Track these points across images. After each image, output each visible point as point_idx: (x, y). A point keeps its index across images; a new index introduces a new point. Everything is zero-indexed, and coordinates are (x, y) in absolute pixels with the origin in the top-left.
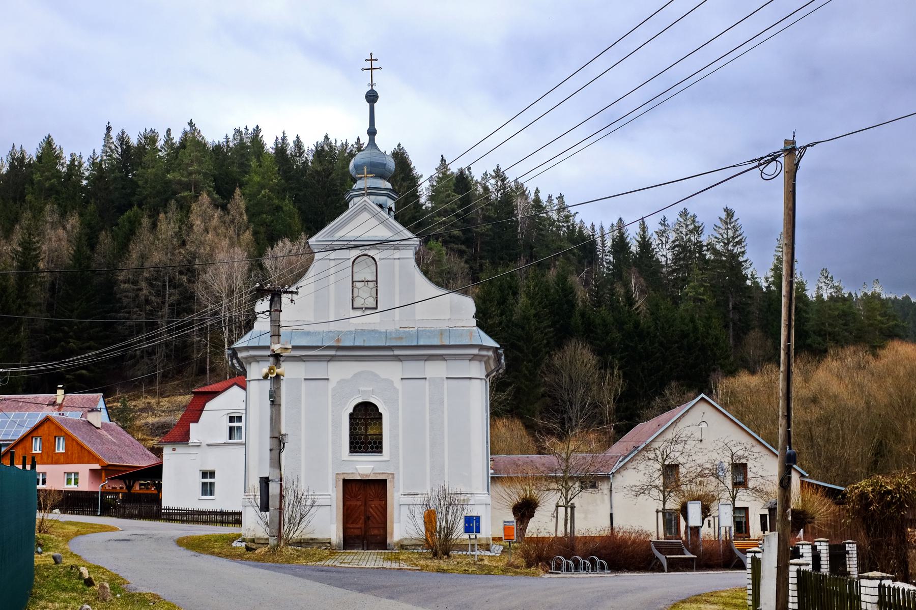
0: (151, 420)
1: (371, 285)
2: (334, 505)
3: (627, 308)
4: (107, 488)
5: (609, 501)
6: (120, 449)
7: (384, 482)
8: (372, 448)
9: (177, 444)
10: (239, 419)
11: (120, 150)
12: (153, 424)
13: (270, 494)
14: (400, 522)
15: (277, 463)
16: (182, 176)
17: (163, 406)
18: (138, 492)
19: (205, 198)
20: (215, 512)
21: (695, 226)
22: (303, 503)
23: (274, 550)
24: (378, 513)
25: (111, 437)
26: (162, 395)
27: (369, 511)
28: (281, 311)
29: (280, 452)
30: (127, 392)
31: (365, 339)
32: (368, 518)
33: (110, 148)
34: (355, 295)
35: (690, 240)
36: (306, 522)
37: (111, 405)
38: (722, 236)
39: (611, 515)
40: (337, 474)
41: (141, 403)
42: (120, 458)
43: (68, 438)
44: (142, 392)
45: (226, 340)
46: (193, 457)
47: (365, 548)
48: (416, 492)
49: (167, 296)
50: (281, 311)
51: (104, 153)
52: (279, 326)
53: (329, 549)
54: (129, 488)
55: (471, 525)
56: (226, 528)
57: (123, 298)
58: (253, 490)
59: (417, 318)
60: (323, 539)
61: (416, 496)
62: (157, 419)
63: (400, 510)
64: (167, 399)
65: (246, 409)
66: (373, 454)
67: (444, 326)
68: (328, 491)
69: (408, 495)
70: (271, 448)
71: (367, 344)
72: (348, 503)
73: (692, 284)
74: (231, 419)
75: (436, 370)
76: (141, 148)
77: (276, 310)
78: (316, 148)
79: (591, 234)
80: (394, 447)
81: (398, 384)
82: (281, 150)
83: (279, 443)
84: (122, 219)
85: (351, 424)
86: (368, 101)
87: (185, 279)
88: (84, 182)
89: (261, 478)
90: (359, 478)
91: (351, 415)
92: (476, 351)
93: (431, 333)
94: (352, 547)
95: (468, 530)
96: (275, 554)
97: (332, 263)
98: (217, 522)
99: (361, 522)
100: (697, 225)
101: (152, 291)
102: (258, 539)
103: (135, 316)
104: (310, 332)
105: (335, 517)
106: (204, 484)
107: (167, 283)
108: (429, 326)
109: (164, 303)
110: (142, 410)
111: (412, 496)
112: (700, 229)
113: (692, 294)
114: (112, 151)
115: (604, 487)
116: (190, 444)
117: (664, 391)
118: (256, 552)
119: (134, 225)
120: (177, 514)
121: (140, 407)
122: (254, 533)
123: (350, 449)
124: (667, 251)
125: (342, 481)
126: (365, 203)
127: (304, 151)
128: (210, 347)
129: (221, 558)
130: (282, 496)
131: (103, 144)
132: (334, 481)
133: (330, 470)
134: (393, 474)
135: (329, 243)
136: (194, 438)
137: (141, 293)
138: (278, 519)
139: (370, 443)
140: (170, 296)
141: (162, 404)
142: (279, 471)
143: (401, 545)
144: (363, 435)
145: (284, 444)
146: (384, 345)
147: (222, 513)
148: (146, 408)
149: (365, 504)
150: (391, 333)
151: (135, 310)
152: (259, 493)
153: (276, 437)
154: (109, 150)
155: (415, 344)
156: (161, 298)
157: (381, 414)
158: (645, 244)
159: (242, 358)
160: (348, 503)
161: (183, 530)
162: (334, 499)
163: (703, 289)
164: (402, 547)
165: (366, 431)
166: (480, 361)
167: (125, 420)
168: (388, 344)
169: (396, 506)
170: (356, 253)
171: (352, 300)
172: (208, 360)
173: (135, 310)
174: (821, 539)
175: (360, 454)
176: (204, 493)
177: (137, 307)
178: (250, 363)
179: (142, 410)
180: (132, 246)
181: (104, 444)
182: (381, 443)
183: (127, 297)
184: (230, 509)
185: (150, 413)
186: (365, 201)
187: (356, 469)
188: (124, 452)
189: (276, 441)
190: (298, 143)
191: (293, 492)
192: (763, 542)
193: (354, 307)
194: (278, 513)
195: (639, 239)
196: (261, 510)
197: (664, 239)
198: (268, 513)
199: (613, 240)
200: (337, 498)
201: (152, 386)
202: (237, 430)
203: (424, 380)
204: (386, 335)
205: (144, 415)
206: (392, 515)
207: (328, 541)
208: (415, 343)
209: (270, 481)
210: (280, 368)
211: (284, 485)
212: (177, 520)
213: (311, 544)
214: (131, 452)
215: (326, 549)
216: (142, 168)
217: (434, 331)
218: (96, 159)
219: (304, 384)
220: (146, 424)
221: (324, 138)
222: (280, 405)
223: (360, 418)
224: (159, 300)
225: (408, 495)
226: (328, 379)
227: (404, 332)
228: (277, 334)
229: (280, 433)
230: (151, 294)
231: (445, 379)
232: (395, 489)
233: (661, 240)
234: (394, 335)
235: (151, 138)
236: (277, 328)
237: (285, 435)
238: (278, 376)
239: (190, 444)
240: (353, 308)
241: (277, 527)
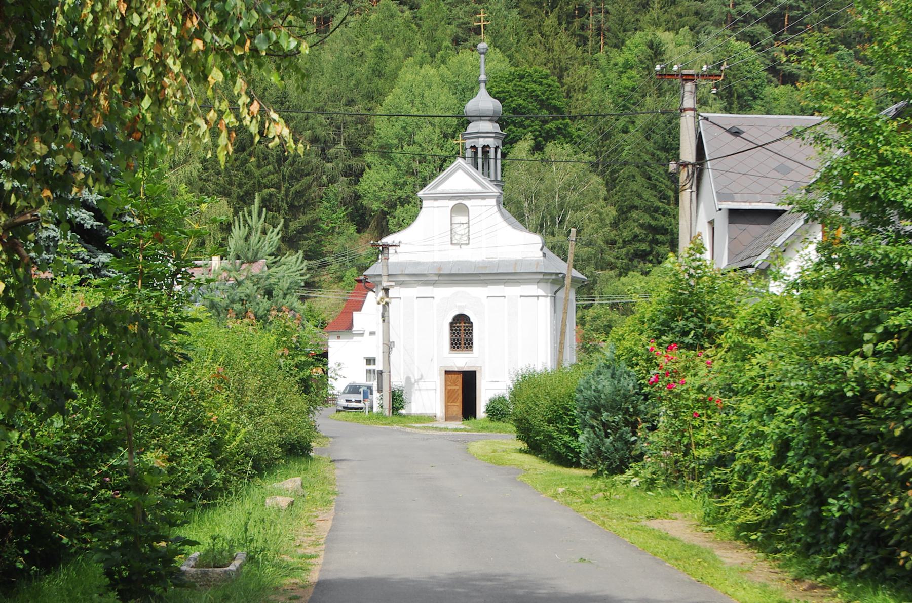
1: (466, 226)
71: (460, 272)
75: (513, 291)
92: (541, 277)
97: (484, 209)
136: (356, 327)
157: (472, 323)
170: (453, 203)
204: (475, 264)
226: (433, 298)
227: (489, 261)
234: (481, 265)
238: (387, 303)
240: (452, 244)
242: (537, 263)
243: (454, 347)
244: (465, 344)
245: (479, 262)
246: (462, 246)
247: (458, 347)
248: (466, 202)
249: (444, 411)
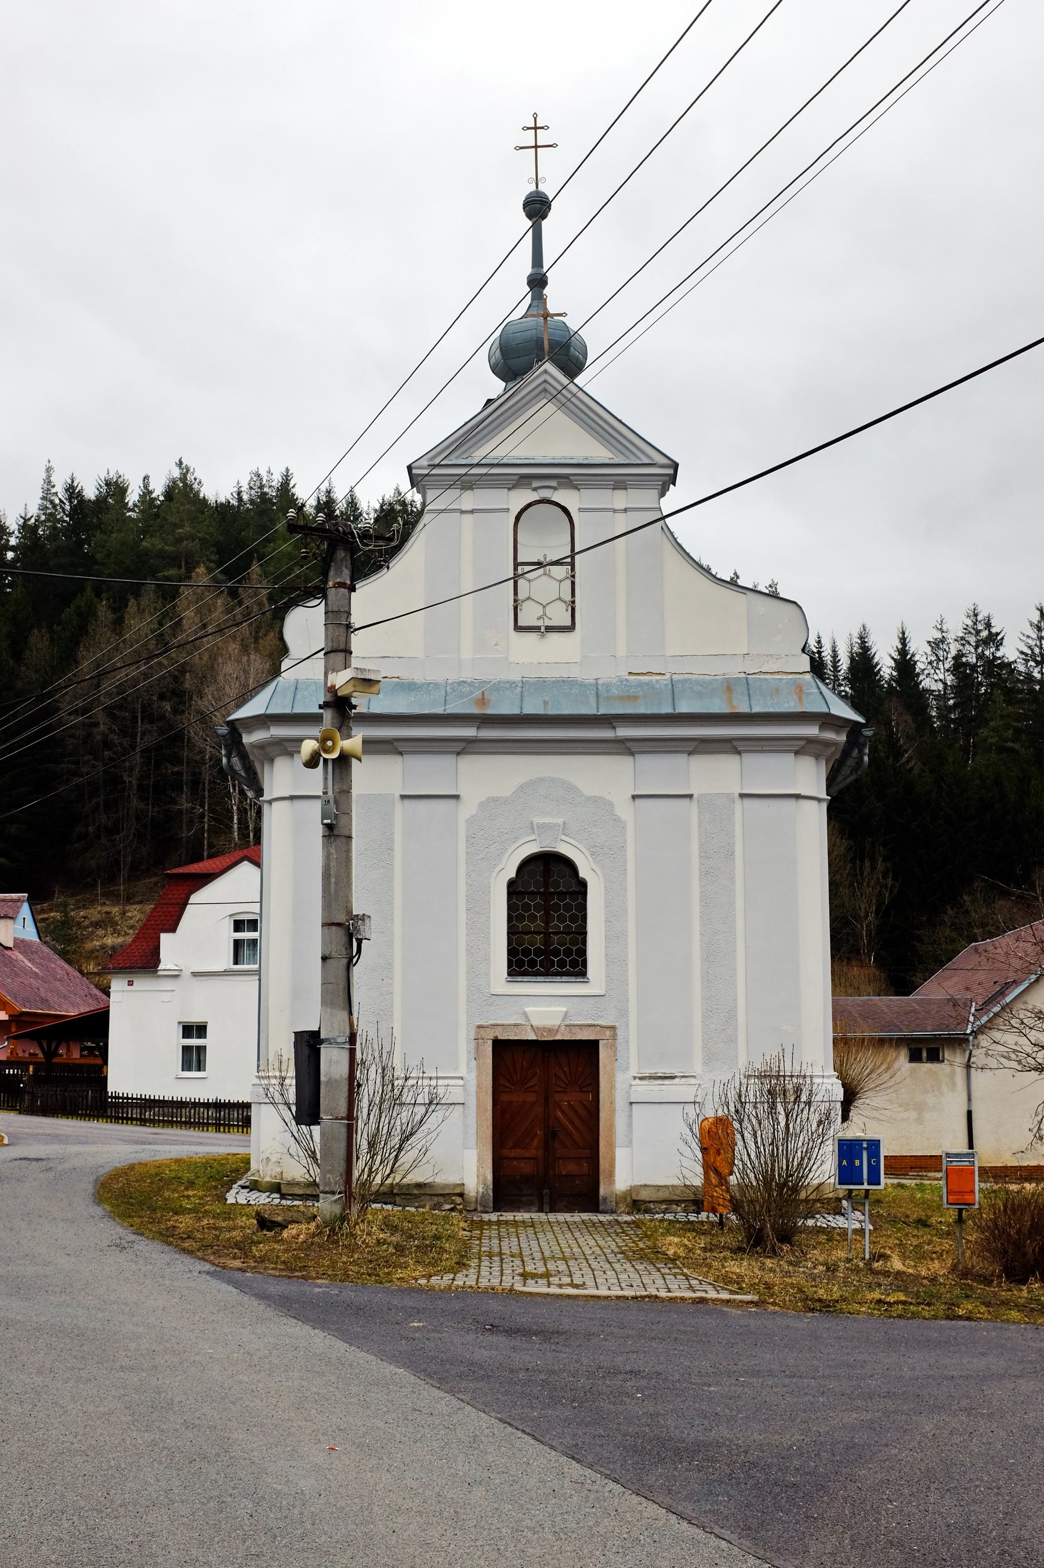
0: (109, 941)
2: (472, 1102)
3: (891, 760)
4: (21, 1054)
5: (965, 1089)
6: (46, 985)
7: (591, 1048)
8: (562, 964)
9: (135, 973)
10: (253, 925)
11: (68, 507)
12: (113, 948)
13: (323, 1078)
14: (630, 1144)
15: (342, 999)
16: (166, 543)
17: (131, 918)
18: (77, 1062)
19: (202, 575)
20: (204, 1103)
21: (990, 633)
22: (407, 1098)
23: (332, 1230)
24: (577, 1122)
25: (30, 965)
26: (129, 899)
27: (557, 1118)
29: (349, 964)
30: (73, 895)
31: (547, 699)
32: (551, 1135)
33: (52, 502)
34: (521, 597)
35: (984, 654)
36: (415, 1151)
37: (46, 916)
38: (1032, 650)
39: (969, 1114)
40: (479, 1027)
41: (94, 913)
42: (44, 1001)
44: (97, 895)
45: (235, 808)
46: (166, 996)
47: (546, 1207)
48: (668, 1071)
49: (139, 734)
51: (42, 510)
52: (348, 626)
53: (461, 1212)
54: (50, 1054)
55: (857, 1163)
56: (226, 1136)
57: (67, 738)
58: (277, 1066)
59: (670, 652)
60: (447, 1186)
61: (667, 1082)
62: (120, 940)
63: (630, 1116)
64: (138, 907)
65: (261, 902)
66: (564, 979)
67: (734, 670)
68: (456, 1069)
69: (650, 1078)
70: (327, 954)
71: (552, 711)
72: (504, 1098)
73: (992, 724)
74: (238, 926)
76: (100, 502)
77: (342, 585)
78: (382, 506)
79: (815, 650)
80: (615, 961)
81: (625, 810)
82: (327, 505)
83: (344, 939)
84: (68, 613)
85: (511, 907)
86: (529, 216)
87: (168, 706)
88: (10, 555)
89: (299, 1035)
90: (532, 1037)
91: (511, 884)
92: (812, 731)
93: (704, 687)
94: (515, 1206)
96: (337, 1242)
98: (208, 1124)
99: (535, 1143)
100: (994, 630)
101: (113, 726)
102: (289, 1184)
103: (85, 770)
104: (415, 684)
105: (474, 1131)
106: (186, 1049)
107: (139, 714)
108: (699, 670)
109: (133, 747)
110: (97, 925)
111: (660, 1082)
112: (999, 638)
113: (993, 740)
114: (54, 506)
115: (954, 1059)
116: (160, 973)
117: (962, 898)
118: (285, 1234)
119: (87, 616)
120: (133, 1106)
121: (93, 919)
122: (279, 1170)
124: (946, 674)
125: (490, 1043)
126: (546, 377)
127: (361, 514)
128: (208, 820)
129: (187, 1260)
130: (353, 1086)
131: (41, 495)
132: (473, 1044)
133: (463, 1018)
134: (613, 1028)
135: (463, 471)
136: (168, 960)
137: (95, 730)
138: (343, 1145)
139: (557, 953)
140: (147, 737)
141: (129, 914)
142: (345, 1015)
143: (635, 1202)
144: (539, 933)
145: (360, 942)
146: (594, 712)
147: (218, 1105)
148: (103, 922)
149: (546, 1100)
150: (608, 686)
151: (85, 758)
152: (292, 1073)
153: (339, 925)
154: (49, 506)
155: (670, 710)
156: (128, 739)
157: (583, 884)
158: (905, 664)
159: (252, 745)
160: (504, 1098)
161: (137, 1142)
162: (473, 1088)
163: (1011, 732)
164: (636, 1204)
165: (547, 923)
166: (817, 757)
167: (69, 940)
168: (602, 711)
169: (620, 1104)
170: (523, 497)
171: (516, 608)
172: (206, 842)
173: (85, 758)
175: (534, 979)
176: (187, 1066)
177: (90, 754)
178: (272, 761)
179: (97, 925)
180: (82, 652)
181: (17, 975)
183: (73, 736)
184: (234, 1098)
185: (110, 930)
186: (546, 372)
187: (525, 1014)
188: (51, 991)
189: (338, 933)
190: (353, 504)
191: (380, 1071)
194: (344, 1130)
195: (896, 656)
196: (299, 1120)
197: (941, 653)
198: (316, 1130)
199: (852, 659)
200: (479, 1086)
201: (114, 885)
202: (249, 946)
203: (687, 801)
204: (597, 690)
205: (100, 932)
206: (611, 1127)
207: (458, 1191)
208: (666, 709)
209: (322, 1042)
210: (349, 736)
211: (358, 1056)
212: (132, 1119)
213: (417, 1196)
214: (66, 992)
215: (452, 1210)
216: (102, 532)
217: (711, 682)
218: (30, 519)
219: (399, 807)
220: (103, 947)
221: (393, 492)
222: (350, 837)
223: (532, 893)
224: (126, 742)
225: (650, 1078)
226: (456, 797)
227: (641, 684)
228: (342, 646)
229: (349, 912)
230: (111, 731)
231: (738, 801)
232: (617, 1064)
233: (937, 655)
234: (615, 691)
235: (116, 489)
236: (343, 630)
237: (363, 918)
239: (160, 973)
240: (518, 628)
241: (341, 1167)
243: (574, 964)
249: (490, 1177)
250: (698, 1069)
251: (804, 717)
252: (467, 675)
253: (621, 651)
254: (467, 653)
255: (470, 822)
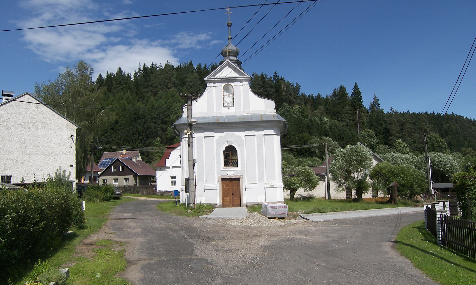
7: (238, 179)
28: (192, 105)
29: (315, 222)
43: (124, 166)
50: (192, 105)
68: (215, 183)
85: (224, 155)
90: (228, 177)
95: (104, 182)
123: (224, 165)
134: (242, 175)
136: (167, 164)
145: (195, 163)
174: (440, 200)
182: (237, 163)
186: (227, 61)
192: (355, 200)
193: (224, 106)
226: (214, 137)
227: (246, 116)
240: (224, 107)
242: (274, 116)
243: (226, 165)
244: (232, 163)
245: (240, 116)
246: (230, 108)
247: (228, 165)
248: (233, 84)
249: (222, 201)
250: (257, 182)
251: (328, 185)
252: (215, 115)
253: (242, 110)
254: (215, 111)
255: (216, 141)
